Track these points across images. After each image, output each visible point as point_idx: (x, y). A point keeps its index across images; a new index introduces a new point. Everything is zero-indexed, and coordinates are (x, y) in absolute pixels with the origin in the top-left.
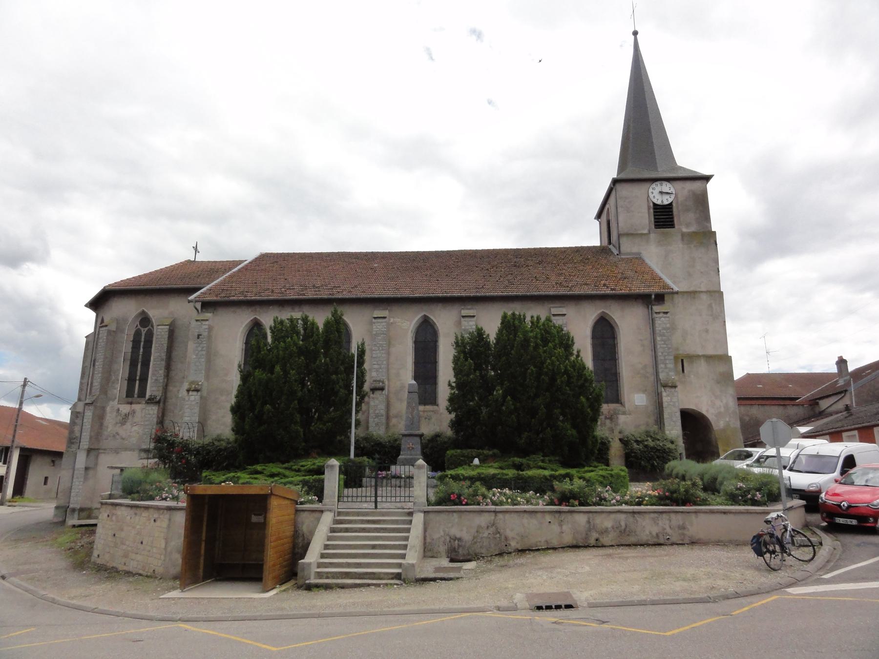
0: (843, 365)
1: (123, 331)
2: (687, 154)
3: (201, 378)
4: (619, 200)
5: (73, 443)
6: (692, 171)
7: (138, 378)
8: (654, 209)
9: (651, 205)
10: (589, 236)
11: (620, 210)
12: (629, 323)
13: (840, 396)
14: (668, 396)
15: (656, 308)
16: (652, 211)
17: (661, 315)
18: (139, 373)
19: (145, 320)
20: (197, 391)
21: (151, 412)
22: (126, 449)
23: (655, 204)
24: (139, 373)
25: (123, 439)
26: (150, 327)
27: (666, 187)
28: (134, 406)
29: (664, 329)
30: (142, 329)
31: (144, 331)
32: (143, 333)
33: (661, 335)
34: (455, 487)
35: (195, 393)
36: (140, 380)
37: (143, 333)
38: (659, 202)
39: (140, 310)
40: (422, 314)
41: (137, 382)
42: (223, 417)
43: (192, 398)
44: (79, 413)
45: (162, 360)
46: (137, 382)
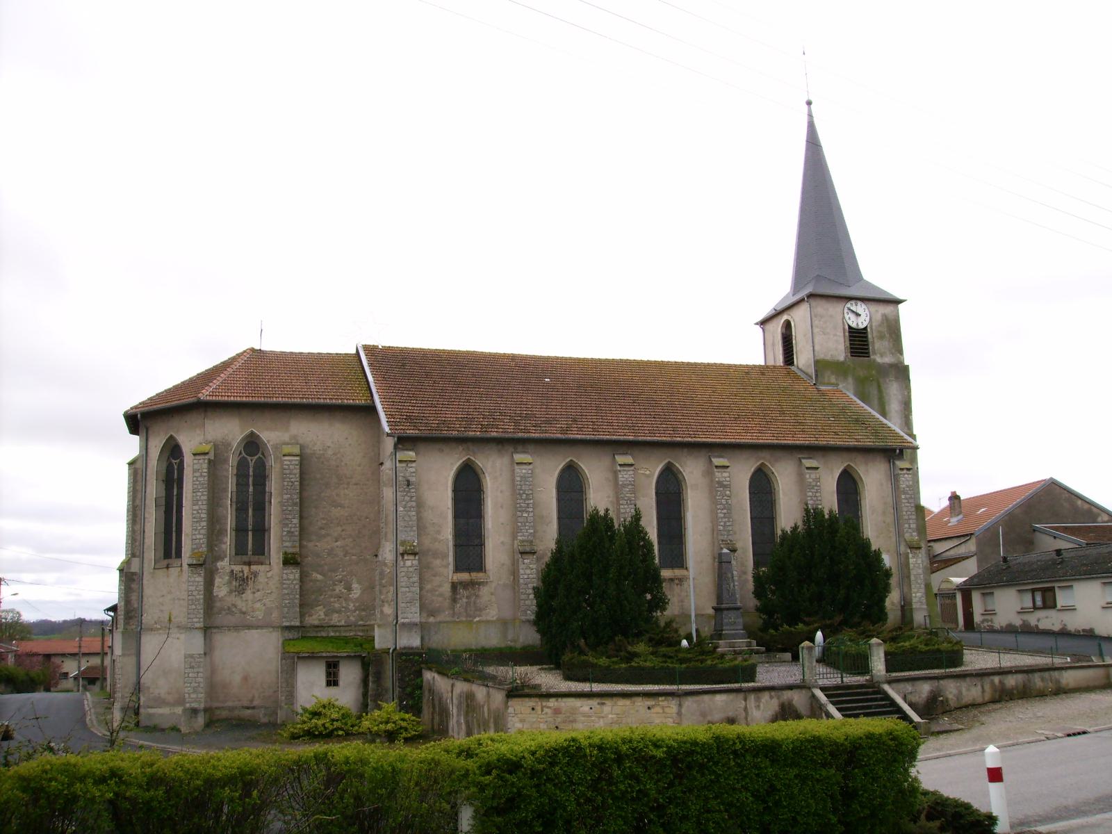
0: (956, 501)
1: (226, 461)
2: (876, 265)
3: (410, 536)
4: (814, 319)
5: (131, 618)
6: (891, 295)
7: (250, 527)
8: (850, 332)
9: (847, 327)
10: (749, 349)
11: (816, 330)
12: (873, 479)
13: (963, 540)
14: (913, 557)
15: (900, 464)
16: (847, 334)
17: (905, 471)
18: (250, 520)
19: (252, 444)
20: (415, 554)
21: (291, 577)
22: (249, 627)
23: (850, 327)
24: (250, 520)
25: (244, 613)
26: (260, 455)
27: (861, 308)
28: (254, 568)
29: (907, 486)
30: (249, 458)
31: (252, 461)
32: (251, 464)
33: (904, 494)
34: (745, 656)
35: (412, 557)
36: (254, 531)
37: (251, 464)
38: (854, 325)
39: (247, 432)
40: (666, 461)
41: (250, 534)
42: (440, 586)
43: (409, 563)
44: (133, 574)
45: (295, 504)
46: (250, 534)
